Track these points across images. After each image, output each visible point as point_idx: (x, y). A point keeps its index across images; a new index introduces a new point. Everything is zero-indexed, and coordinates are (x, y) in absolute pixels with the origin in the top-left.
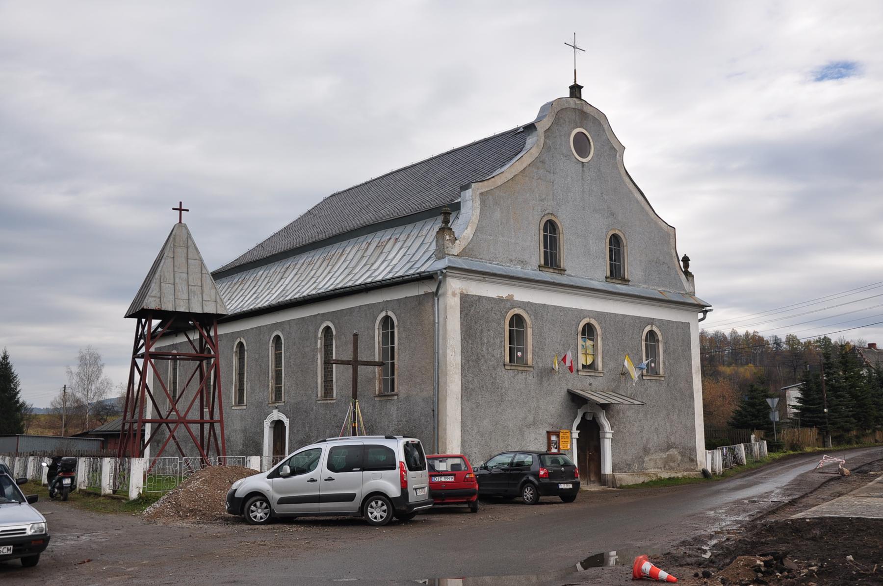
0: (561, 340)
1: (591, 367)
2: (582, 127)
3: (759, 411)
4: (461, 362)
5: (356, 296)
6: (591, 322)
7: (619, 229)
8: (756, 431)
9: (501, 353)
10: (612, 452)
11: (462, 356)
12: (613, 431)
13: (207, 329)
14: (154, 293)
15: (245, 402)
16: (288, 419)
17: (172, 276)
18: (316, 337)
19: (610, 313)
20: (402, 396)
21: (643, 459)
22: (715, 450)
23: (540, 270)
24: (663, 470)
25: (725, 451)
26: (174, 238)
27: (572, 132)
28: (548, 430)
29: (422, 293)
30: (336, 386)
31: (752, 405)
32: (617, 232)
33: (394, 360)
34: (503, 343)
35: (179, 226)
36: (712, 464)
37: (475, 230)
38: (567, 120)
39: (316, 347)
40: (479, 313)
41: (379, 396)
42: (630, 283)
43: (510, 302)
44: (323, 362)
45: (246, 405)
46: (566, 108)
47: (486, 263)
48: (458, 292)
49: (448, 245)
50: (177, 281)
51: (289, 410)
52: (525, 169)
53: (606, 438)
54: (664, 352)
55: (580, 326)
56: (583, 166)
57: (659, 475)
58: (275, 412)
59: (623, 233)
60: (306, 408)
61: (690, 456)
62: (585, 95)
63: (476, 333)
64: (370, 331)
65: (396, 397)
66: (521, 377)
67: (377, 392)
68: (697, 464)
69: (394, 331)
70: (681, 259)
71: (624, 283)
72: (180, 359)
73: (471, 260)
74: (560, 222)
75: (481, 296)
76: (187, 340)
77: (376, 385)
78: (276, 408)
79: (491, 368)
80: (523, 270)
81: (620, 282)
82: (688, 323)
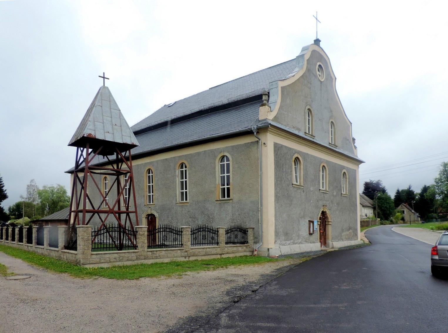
0: (313, 173)
2: (321, 62)
17: (101, 118)
20: (235, 200)
30: (189, 195)
35: (104, 87)
39: (175, 175)
50: (105, 121)
51: (158, 208)
56: (321, 83)
62: (322, 44)
65: (231, 201)
82: (356, 170)
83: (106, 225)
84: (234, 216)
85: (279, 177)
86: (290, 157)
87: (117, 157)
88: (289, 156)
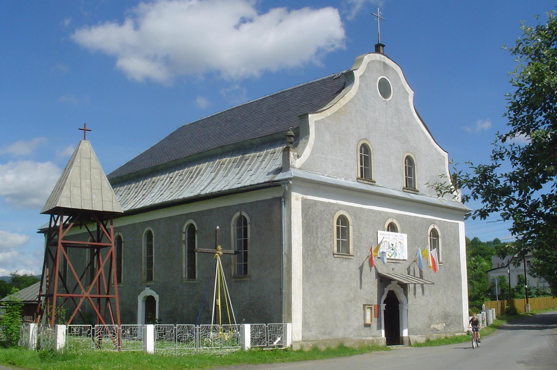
4: (303, 251)
5: (178, 207)
6: (394, 222)
7: (412, 152)
9: (331, 244)
11: (303, 247)
13: (104, 224)
15: (122, 281)
16: (158, 295)
18: (181, 232)
23: (358, 182)
28: (364, 304)
32: (410, 155)
33: (247, 249)
34: (332, 237)
41: (235, 277)
44: (187, 251)
45: (123, 284)
46: (374, 61)
47: (320, 175)
49: (292, 161)
52: (346, 104)
54: (442, 245)
55: (386, 225)
58: (148, 289)
59: (413, 155)
66: (345, 263)
67: (233, 275)
69: (247, 228)
72: (69, 247)
73: (309, 172)
74: (371, 146)
75: (316, 200)
76: (87, 231)
77: (232, 269)
78: (148, 286)
80: (345, 181)
83: (40, 230)
87: (97, 229)
88: (327, 215)
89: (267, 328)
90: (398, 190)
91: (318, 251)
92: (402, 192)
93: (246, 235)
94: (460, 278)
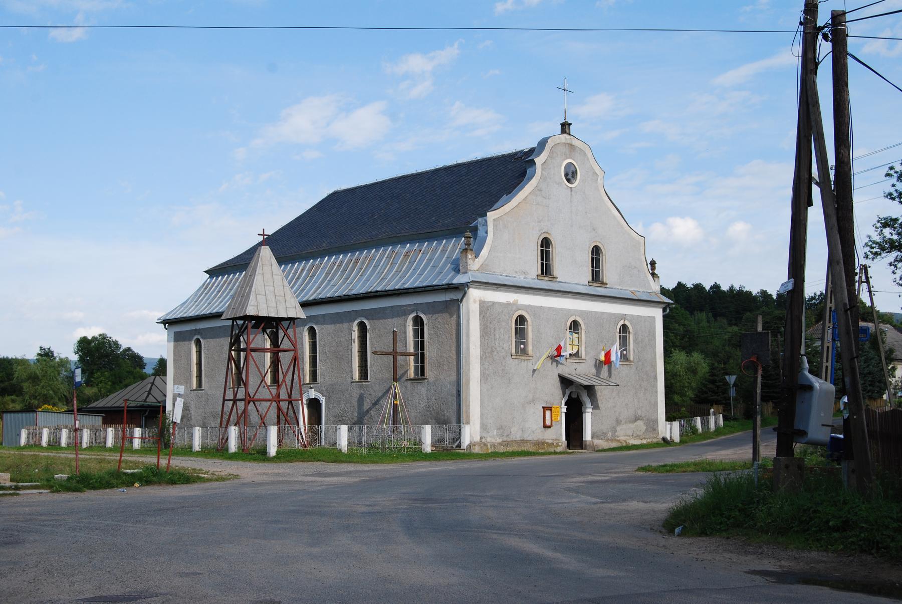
1: (576, 355)
2: (571, 158)
3: (718, 387)
7: (600, 241)
8: (714, 406)
10: (592, 423)
12: (592, 407)
14: (253, 302)
16: (324, 397)
17: (263, 289)
19: (592, 311)
21: (615, 429)
22: (673, 422)
24: (631, 437)
25: (682, 423)
26: (262, 259)
27: (563, 162)
28: (543, 406)
29: (448, 299)
31: (713, 382)
32: (598, 244)
34: (510, 338)
36: (671, 433)
37: (489, 249)
38: (559, 153)
40: (493, 315)
42: (608, 286)
43: (515, 305)
46: (558, 144)
48: (478, 299)
52: (527, 197)
53: (139, 438)
54: (634, 341)
56: (571, 191)
57: (628, 441)
60: (341, 389)
61: (652, 425)
63: (490, 331)
64: (402, 327)
68: (658, 433)
70: (649, 263)
71: (603, 285)
79: (502, 358)
81: (599, 285)
84: (430, 402)
85: (488, 347)
86: (508, 318)
88: (505, 315)
89: (446, 428)
90: (583, 285)
91: (495, 353)
92: (587, 287)
93: (422, 336)
94: (655, 378)
